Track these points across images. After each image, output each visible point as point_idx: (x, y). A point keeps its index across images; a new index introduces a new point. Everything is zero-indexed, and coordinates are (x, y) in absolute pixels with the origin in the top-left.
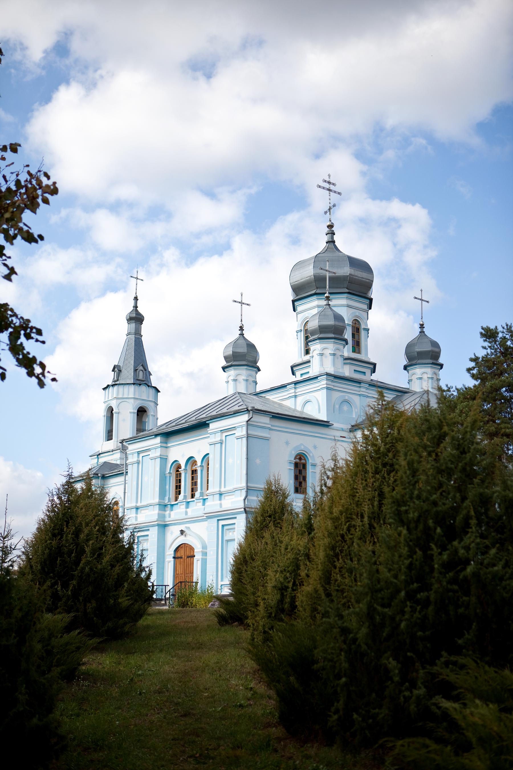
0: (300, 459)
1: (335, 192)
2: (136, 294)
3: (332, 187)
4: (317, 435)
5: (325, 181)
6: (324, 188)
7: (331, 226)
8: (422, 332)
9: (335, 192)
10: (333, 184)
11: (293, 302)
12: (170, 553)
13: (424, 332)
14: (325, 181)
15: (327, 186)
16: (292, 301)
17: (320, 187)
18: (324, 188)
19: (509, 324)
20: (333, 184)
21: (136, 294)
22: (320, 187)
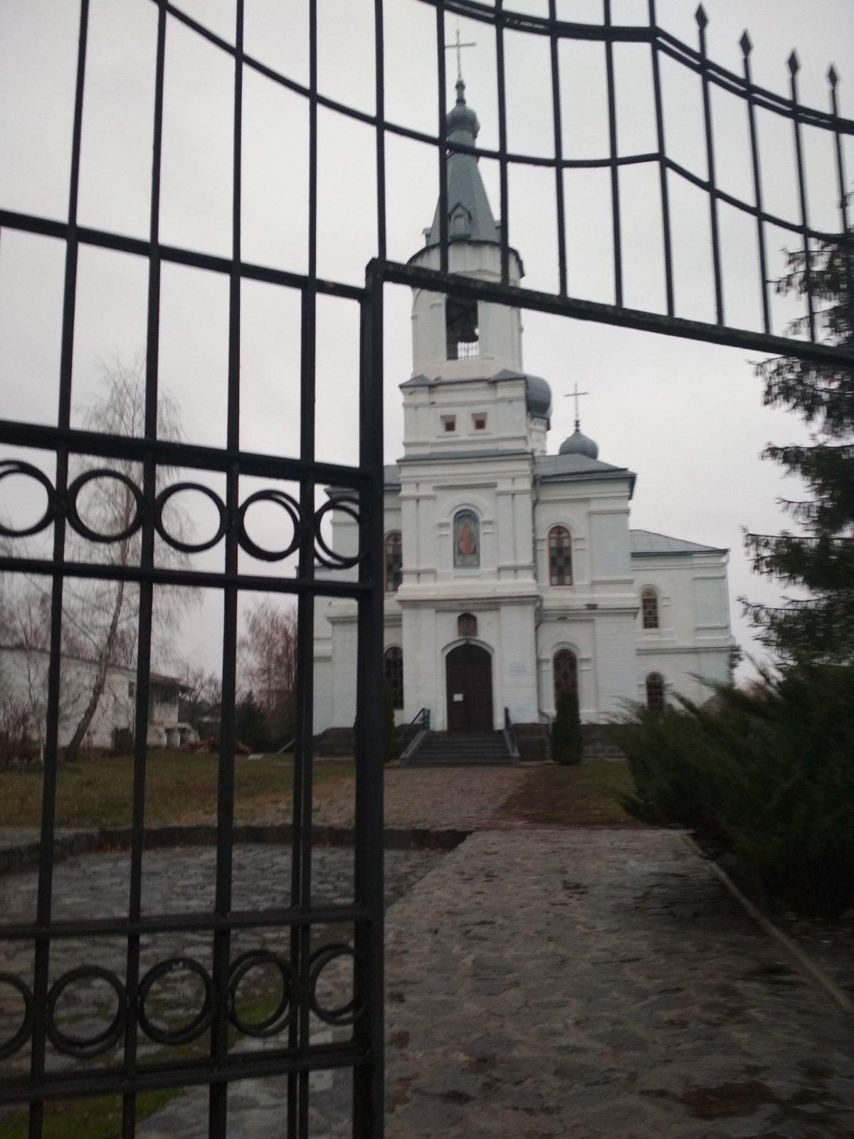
2: (577, 415)
8: (577, 431)
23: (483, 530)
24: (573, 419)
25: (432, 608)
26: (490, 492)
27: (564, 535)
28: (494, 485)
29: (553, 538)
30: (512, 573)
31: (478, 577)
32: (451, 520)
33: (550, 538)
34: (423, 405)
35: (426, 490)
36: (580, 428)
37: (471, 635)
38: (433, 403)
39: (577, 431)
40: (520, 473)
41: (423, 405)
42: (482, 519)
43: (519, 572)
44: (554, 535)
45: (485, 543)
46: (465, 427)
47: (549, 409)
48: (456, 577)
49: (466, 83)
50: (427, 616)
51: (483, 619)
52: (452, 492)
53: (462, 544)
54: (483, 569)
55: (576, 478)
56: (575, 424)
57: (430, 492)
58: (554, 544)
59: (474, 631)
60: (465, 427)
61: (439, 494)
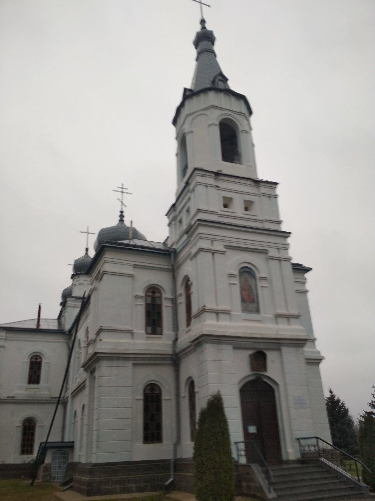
0: (153, 292)
1: (127, 193)
2: (87, 245)
3: (124, 190)
4: (313, 361)
5: (119, 188)
6: (118, 191)
7: (122, 212)
8: (87, 254)
9: (127, 193)
10: (126, 189)
11: (188, 95)
12: (189, 252)
13: (88, 254)
14: (119, 188)
15: (120, 190)
16: (185, 90)
17: (115, 191)
18: (118, 191)
19: (369, 404)
20: (126, 189)
21: (87, 245)
22: (115, 191)
23: (260, 284)
24: (85, 247)
25: (230, 344)
26: (262, 256)
27: (157, 295)
28: (265, 252)
29: (149, 296)
30: (285, 320)
31: (259, 321)
32: (236, 272)
33: (146, 295)
34: (212, 186)
35: (218, 246)
36: (89, 253)
37: (261, 371)
38: (217, 186)
39: (87, 254)
40: (282, 246)
41: (212, 186)
42: (258, 275)
43: (221, 316)
44: (150, 294)
45: (263, 295)
46: (238, 208)
47: (137, 232)
48: (245, 320)
49: (206, 20)
50: (227, 352)
51: (271, 356)
52: (236, 252)
53: (244, 293)
54: (263, 314)
55: (274, 258)
56: (85, 250)
57: (222, 248)
58: (149, 301)
59: (264, 367)
60: (238, 208)
61: (229, 252)
